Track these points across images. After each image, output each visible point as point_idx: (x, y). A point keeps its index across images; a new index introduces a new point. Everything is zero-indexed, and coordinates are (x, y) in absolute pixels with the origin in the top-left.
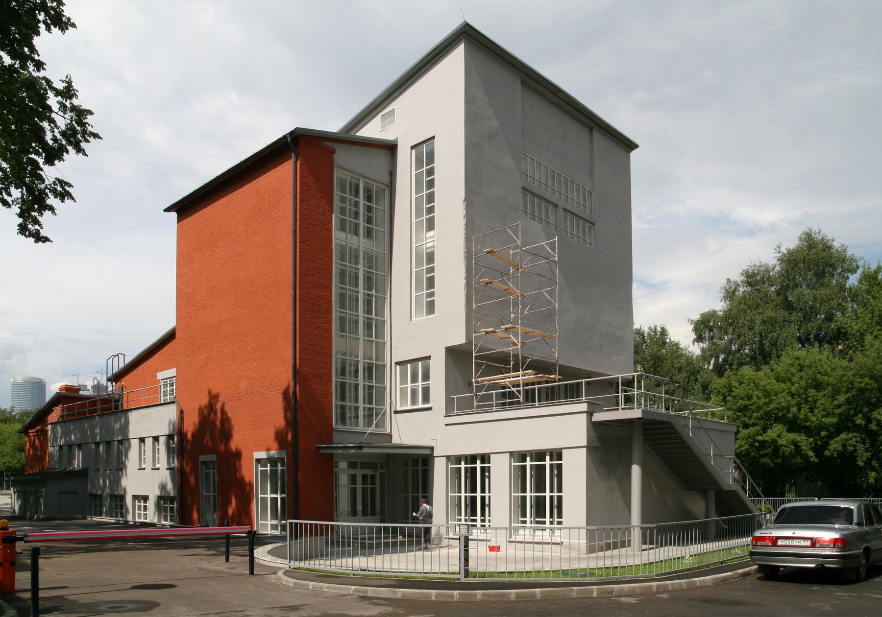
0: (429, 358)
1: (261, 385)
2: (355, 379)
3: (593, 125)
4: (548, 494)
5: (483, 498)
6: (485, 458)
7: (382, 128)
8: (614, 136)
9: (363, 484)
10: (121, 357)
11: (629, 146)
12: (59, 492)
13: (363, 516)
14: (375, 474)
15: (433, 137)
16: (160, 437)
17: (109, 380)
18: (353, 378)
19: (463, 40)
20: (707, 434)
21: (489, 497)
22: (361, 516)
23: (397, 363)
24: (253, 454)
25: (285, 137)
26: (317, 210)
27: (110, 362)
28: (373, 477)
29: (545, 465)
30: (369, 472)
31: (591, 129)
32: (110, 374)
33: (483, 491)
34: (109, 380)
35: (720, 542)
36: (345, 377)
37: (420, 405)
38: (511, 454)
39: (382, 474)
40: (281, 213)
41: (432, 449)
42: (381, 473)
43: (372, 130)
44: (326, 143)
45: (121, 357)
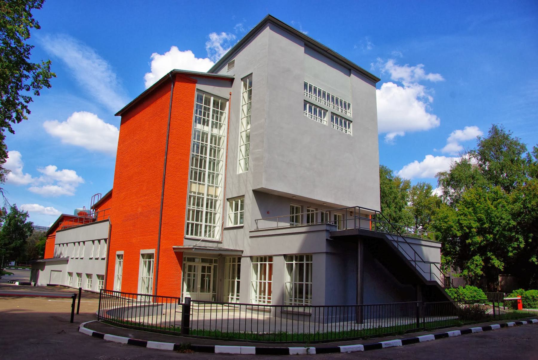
0: (243, 196)
1: (147, 210)
2: (197, 207)
3: (351, 68)
4: (304, 283)
5: (307, 285)
6: (270, 258)
7: (228, 70)
8: (370, 77)
9: (202, 272)
10: (100, 195)
11: (375, 80)
12: (52, 271)
13: (201, 292)
14: (210, 266)
15: (252, 73)
16: (101, 240)
17: (92, 208)
18: (196, 207)
19: (269, 24)
20: (410, 246)
21: (311, 284)
22: (200, 292)
23: (227, 199)
24: (140, 251)
25: (168, 74)
26: (183, 112)
27: (93, 197)
28: (209, 268)
29: (303, 263)
30: (207, 265)
31: (350, 70)
32: (92, 205)
33: (307, 281)
34: (92, 208)
35: (154, 322)
36: (199, 207)
37: (239, 225)
38: (285, 256)
39: (215, 266)
40: (165, 114)
41: (242, 252)
42: (214, 265)
43: (224, 72)
44: (192, 78)
45: (100, 195)
